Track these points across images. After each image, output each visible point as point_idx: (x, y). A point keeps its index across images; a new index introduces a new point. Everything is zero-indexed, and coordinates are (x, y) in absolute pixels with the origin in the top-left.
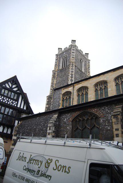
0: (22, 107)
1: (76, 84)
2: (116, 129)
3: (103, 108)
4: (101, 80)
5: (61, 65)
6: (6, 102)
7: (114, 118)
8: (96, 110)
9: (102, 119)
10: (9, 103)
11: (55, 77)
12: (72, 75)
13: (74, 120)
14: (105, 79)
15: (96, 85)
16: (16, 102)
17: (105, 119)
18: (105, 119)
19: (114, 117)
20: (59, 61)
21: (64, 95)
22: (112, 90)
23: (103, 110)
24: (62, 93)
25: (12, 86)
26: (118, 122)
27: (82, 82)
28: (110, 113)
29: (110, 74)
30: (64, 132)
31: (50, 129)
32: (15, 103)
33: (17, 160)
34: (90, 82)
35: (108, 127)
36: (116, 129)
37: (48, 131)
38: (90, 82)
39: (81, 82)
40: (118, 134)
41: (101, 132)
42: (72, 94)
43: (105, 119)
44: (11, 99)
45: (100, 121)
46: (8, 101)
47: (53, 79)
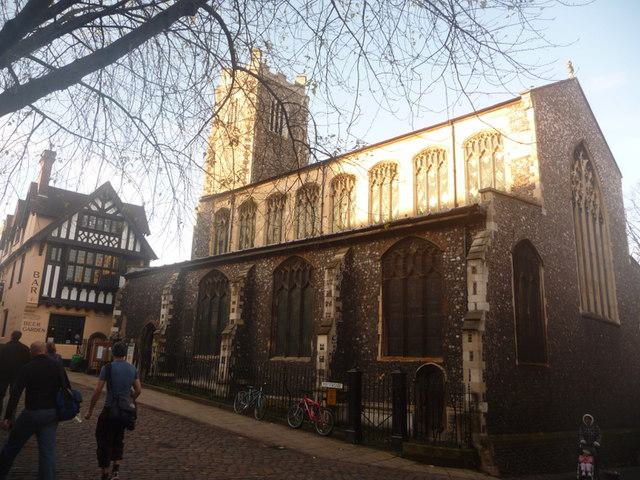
0: (130, 248)
6: (96, 242)
10: (90, 241)
13: (276, 272)
25: (103, 206)
32: (114, 244)
42: (320, 192)
44: (105, 234)
46: (88, 237)
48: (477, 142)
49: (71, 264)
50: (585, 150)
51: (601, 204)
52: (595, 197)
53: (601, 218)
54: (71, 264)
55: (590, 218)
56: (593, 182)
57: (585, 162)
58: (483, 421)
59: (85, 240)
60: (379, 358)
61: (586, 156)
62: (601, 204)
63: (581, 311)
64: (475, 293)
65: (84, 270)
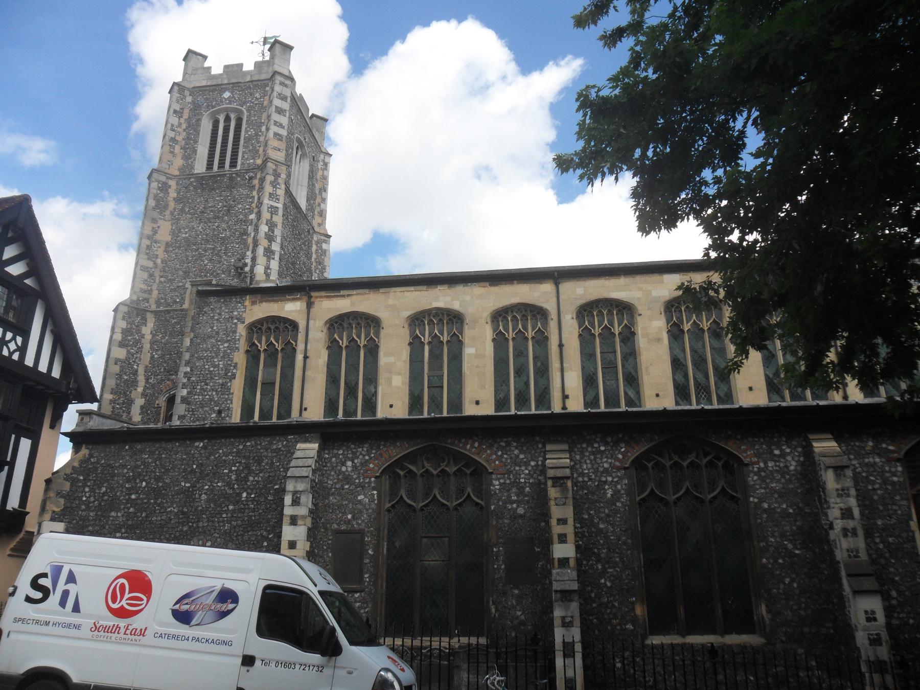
1: (323, 293)
2: (559, 520)
3: (503, 444)
4: (440, 304)
5: (203, 150)
7: (553, 486)
8: (476, 445)
9: (498, 479)
11: (166, 207)
12: (272, 225)
14: (456, 306)
15: (417, 320)
16: (19, 340)
17: (508, 482)
18: (510, 479)
19: (553, 483)
20: (193, 127)
21: (256, 328)
22: (480, 356)
23: (502, 448)
24: (249, 320)
26: (566, 498)
27: (355, 292)
28: (527, 464)
29: (477, 290)
30: (345, 514)
31: (296, 502)
33: (146, 628)
34: (390, 302)
35: (518, 506)
36: (559, 520)
37: (288, 511)
38: (390, 302)
39: (350, 292)
40: (564, 536)
41: (494, 522)
42: (301, 337)
43: (510, 479)
45: (491, 484)
47: (155, 214)
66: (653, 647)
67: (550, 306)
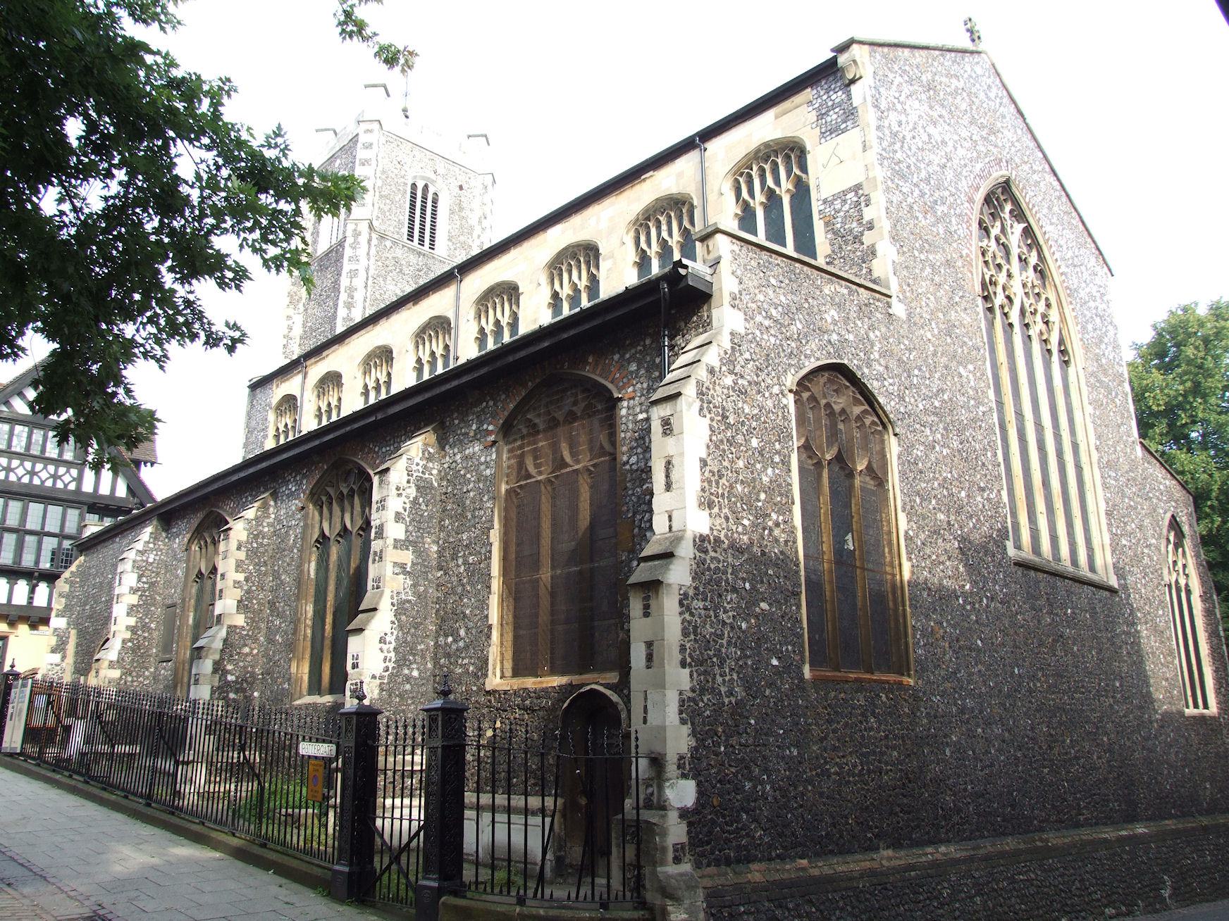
37: (117, 592)
46: (32, 473)
48: (755, 173)
49: (11, 530)
50: (1016, 202)
51: (1063, 319)
52: (1048, 306)
53: (1063, 352)
54: (11, 530)
55: (1036, 347)
56: (1041, 272)
57: (1019, 228)
58: (676, 832)
59: (72, 487)
60: (494, 681)
61: (1019, 214)
62: (1063, 319)
63: (1011, 551)
64: (668, 487)
65: (40, 543)
66: (299, 708)
67: (691, 189)
